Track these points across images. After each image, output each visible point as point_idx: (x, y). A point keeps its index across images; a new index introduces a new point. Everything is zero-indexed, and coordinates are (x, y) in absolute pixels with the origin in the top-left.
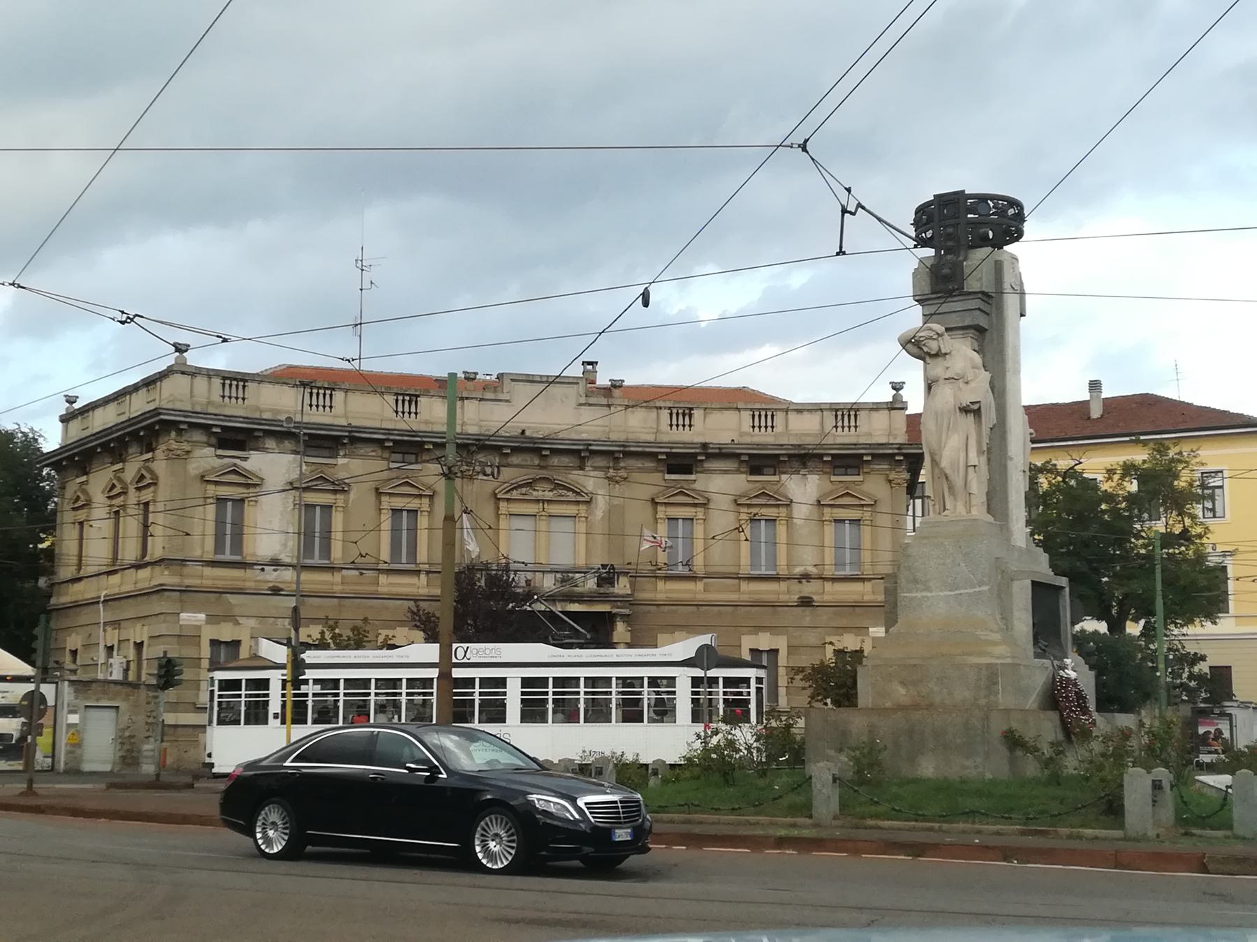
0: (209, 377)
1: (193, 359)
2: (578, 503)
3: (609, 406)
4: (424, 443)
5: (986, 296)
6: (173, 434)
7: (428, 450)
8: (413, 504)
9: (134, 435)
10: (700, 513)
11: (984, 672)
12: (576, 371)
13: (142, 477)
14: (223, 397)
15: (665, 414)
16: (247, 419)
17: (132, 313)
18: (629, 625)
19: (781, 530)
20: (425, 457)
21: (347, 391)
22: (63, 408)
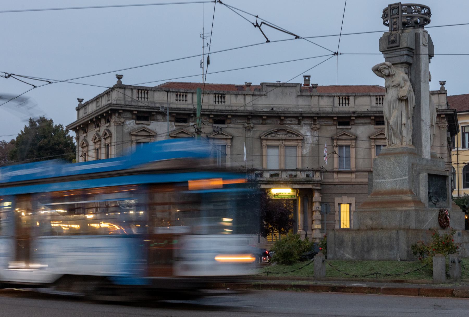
0: (132, 89)
1: (124, 82)
2: (297, 140)
3: (311, 96)
4: (227, 115)
5: (410, 49)
6: (117, 115)
7: (230, 118)
8: (223, 142)
9: (102, 115)
10: (353, 143)
11: (403, 213)
12: (301, 81)
13: (106, 134)
14: (138, 98)
15: (336, 99)
16: (148, 107)
17: (10, 73)
18: (321, 194)
19: (352, 150)
20: (229, 121)
21: (193, 93)
22: (77, 104)
